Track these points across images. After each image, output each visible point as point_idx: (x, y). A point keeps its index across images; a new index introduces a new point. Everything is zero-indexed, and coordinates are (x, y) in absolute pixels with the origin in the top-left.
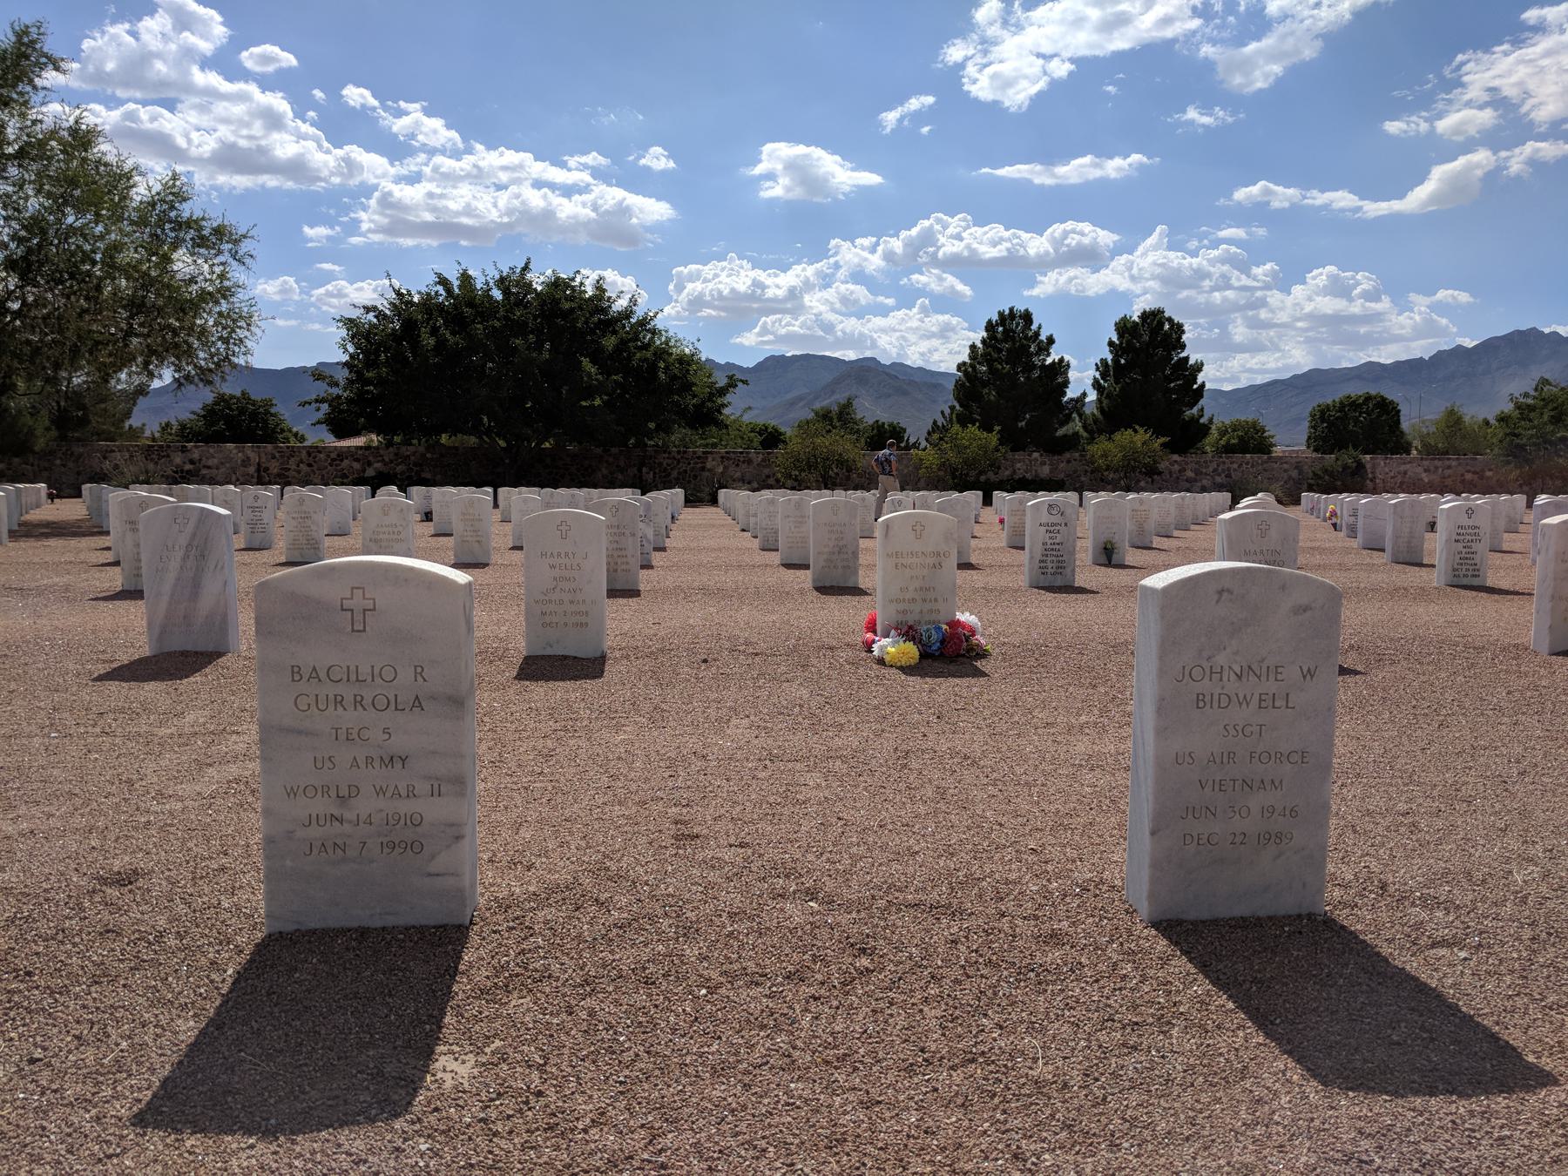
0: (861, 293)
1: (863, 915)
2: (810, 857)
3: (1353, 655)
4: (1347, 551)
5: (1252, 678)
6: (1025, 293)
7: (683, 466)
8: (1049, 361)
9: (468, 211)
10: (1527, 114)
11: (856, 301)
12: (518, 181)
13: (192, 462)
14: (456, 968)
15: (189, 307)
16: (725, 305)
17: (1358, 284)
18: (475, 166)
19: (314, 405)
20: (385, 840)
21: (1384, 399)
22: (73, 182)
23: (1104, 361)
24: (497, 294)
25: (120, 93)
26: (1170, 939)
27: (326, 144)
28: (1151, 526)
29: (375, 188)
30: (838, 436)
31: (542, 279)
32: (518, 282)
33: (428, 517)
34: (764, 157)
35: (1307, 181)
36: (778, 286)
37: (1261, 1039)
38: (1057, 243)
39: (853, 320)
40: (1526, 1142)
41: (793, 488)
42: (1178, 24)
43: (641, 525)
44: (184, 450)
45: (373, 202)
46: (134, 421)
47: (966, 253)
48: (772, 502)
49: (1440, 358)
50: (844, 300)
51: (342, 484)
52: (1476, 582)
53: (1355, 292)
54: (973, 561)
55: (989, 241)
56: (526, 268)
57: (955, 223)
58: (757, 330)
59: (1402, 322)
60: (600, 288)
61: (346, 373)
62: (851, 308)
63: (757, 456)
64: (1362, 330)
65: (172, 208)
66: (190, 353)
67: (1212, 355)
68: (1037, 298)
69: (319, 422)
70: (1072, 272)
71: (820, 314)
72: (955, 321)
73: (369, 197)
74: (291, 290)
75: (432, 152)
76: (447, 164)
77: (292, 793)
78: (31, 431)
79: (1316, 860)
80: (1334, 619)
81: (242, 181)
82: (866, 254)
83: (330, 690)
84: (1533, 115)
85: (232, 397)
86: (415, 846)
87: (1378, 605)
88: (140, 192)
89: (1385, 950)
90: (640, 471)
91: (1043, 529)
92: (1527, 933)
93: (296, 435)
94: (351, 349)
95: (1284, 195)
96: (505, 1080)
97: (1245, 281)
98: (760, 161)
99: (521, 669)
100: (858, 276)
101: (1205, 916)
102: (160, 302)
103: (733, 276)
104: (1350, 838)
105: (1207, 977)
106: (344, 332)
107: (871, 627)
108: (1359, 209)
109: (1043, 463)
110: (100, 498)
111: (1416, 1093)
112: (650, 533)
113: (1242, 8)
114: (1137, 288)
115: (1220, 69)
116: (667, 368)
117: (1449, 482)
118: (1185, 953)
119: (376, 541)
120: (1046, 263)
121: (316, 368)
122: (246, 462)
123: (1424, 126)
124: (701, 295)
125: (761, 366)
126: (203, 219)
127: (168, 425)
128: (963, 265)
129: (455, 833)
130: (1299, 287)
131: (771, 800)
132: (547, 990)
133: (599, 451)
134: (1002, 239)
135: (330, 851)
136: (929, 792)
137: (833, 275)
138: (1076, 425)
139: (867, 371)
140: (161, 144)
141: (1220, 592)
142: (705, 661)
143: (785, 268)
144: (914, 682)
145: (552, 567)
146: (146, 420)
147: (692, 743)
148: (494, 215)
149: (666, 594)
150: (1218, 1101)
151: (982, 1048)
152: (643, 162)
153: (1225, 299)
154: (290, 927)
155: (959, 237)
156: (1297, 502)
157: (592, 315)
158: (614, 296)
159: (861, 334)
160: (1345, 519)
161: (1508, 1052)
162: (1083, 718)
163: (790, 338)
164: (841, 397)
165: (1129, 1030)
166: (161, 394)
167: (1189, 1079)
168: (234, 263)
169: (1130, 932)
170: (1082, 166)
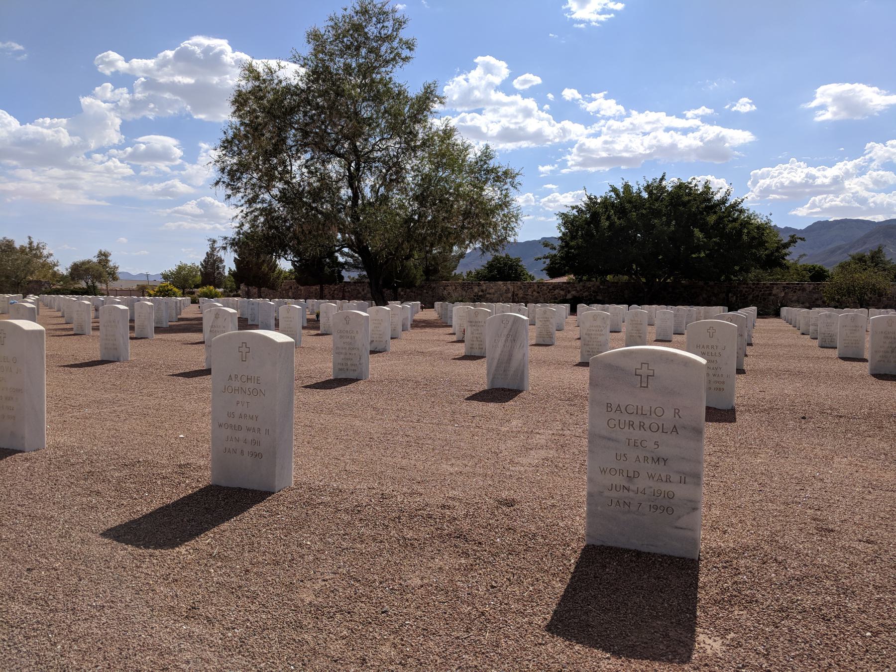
9: (626, 149)
11: (885, 182)
13: (482, 291)
18: (631, 124)
20: (652, 504)
22: (443, 156)
24: (645, 195)
25: (459, 110)
27: (553, 122)
29: (576, 142)
32: (657, 187)
34: (818, 95)
36: (825, 177)
39: (882, 195)
41: (836, 307)
44: (479, 285)
45: (574, 150)
46: (457, 271)
48: (854, 319)
50: (876, 182)
56: (662, 179)
58: (808, 205)
63: (809, 286)
65: (485, 163)
66: (489, 236)
71: (857, 192)
73: (572, 147)
74: (531, 200)
75: (608, 119)
76: (615, 124)
77: (603, 471)
78: (415, 277)
81: (510, 146)
83: (626, 418)
85: (501, 257)
86: (669, 510)
88: (471, 157)
90: (727, 295)
94: (563, 229)
98: (815, 98)
103: (795, 172)
106: (560, 221)
110: (447, 309)
116: (748, 233)
122: (507, 291)
124: (769, 186)
125: (810, 229)
127: (470, 272)
133: (701, 283)
135: (622, 505)
137: (868, 166)
140: (476, 132)
142: (804, 418)
143: (831, 165)
146: (461, 270)
148: (641, 150)
149: (763, 373)
152: (734, 109)
154: (598, 543)
163: (831, 210)
166: (471, 257)
168: (512, 188)
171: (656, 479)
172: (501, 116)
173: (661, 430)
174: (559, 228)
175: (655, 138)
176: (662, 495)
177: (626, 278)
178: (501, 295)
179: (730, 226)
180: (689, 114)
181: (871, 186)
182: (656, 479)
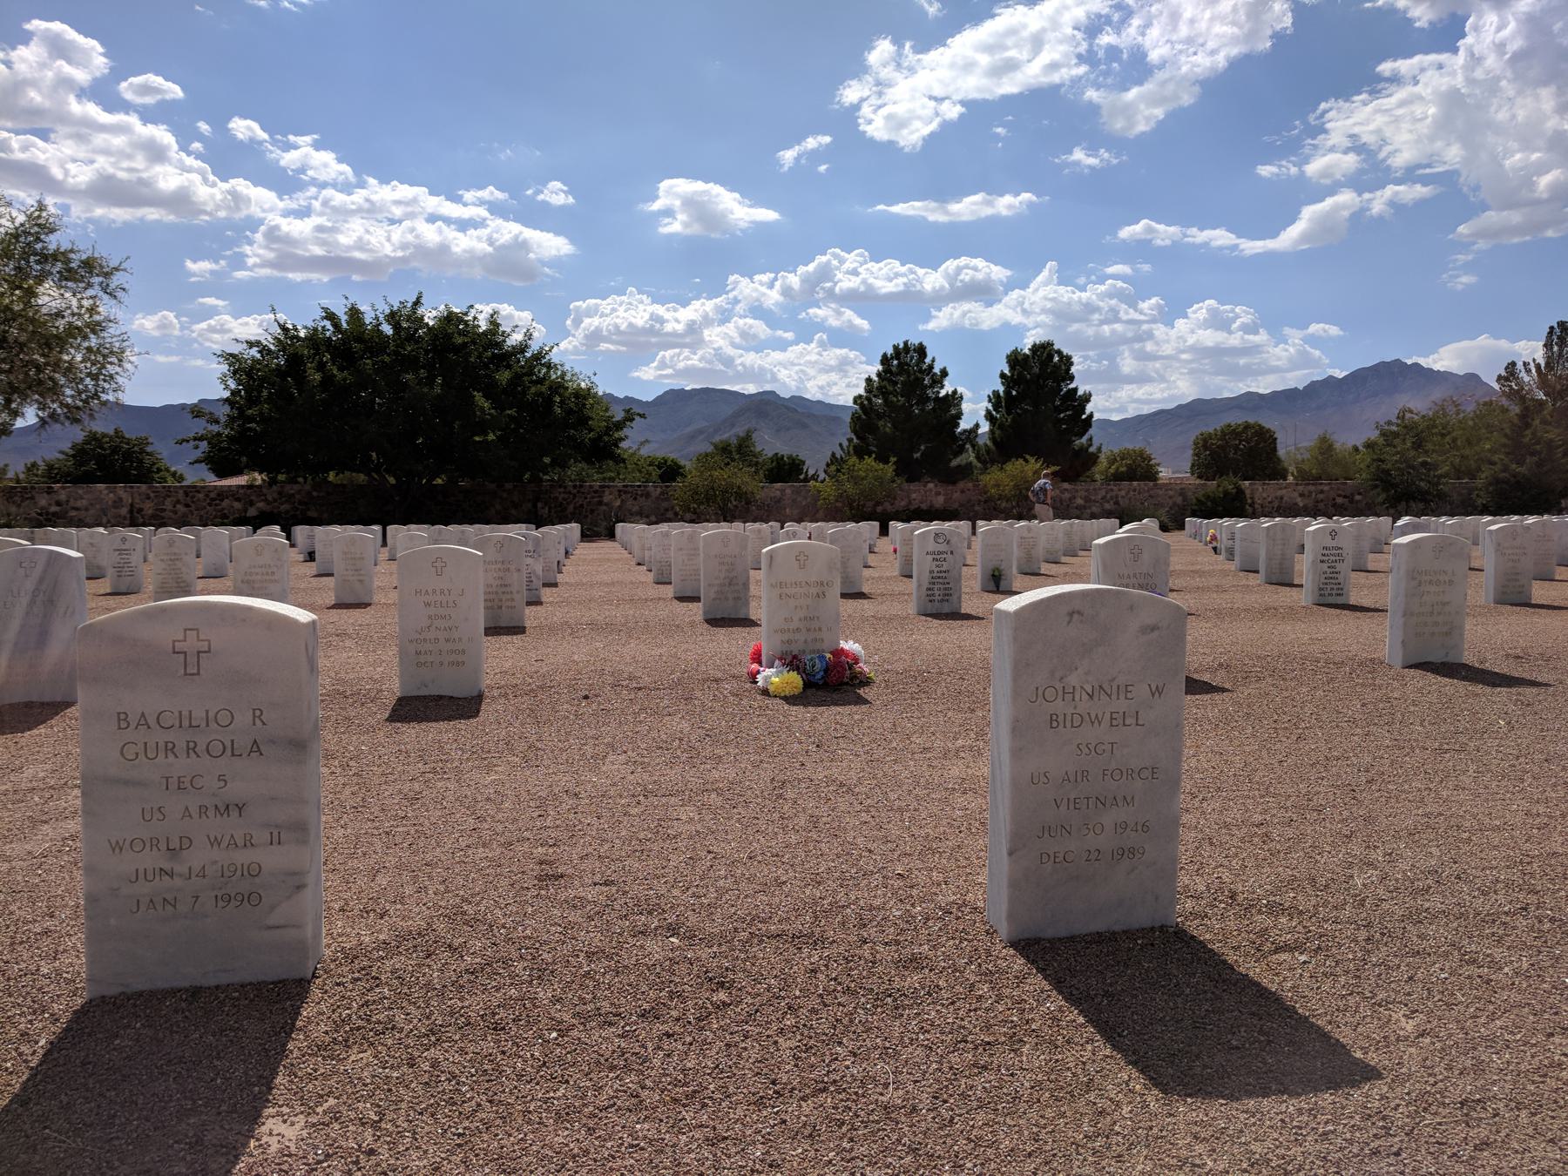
0: (760, 328)
1: (724, 948)
2: (676, 892)
3: (1222, 673)
4: (1225, 573)
5: (1104, 697)
6: (921, 327)
7: (579, 500)
8: (943, 393)
10: (1384, 160)
11: (755, 336)
12: (411, 216)
13: (58, 504)
14: (293, 1025)
15: (54, 342)
16: (625, 339)
17: (1238, 317)
18: (367, 200)
19: (192, 443)
23: (996, 393)
24: (387, 329)
26: (1027, 958)
27: (212, 178)
28: (1040, 552)
29: (261, 222)
30: (738, 466)
31: (434, 313)
33: (311, 557)
35: (1186, 223)
36: (677, 321)
37: (1108, 1052)
38: (952, 279)
40: (1348, 1136)
42: (1064, 70)
43: (529, 561)
44: (50, 491)
45: (259, 237)
47: (862, 289)
48: (667, 535)
49: (1313, 388)
50: (744, 334)
51: (222, 524)
52: (1340, 600)
53: (1234, 326)
54: (865, 590)
55: (886, 276)
56: (417, 303)
57: (852, 259)
59: (1280, 354)
60: (494, 323)
61: (227, 409)
62: (750, 342)
63: (655, 489)
64: (1242, 362)
65: (38, 240)
66: (55, 390)
67: (1101, 387)
68: (932, 332)
69: (197, 461)
70: (966, 306)
72: (852, 355)
73: (255, 231)
75: (323, 185)
76: (339, 198)
77: (117, 847)
79: (1168, 871)
80: (1180, 638)
81: (120, 214)
82: (763, 289)
84: (1389, 162)
85: (104, 435)
86: (251, 898)
89: (1231, 958)
90: (535, 506)
91: (930, 557)
92: (1363, 935)
93: (174, 474)
95: (1166, 232)
96: (335, 1141)
98: (656, 197)
99: (393, 710)
100: (757, 311)
101: (1063, 933)
102: (23, 338)
103: (633, 310)
104: (1207, 850)
105: (1060, 992)
106: (225, 368)
107: (757, 658)
108: (1236, 247)
109: (938, 494)
111: (1250, 1095)
112: (539, 568)
113: (1125, 56)
114: (1029, 322)
115: (1104, 112)
116: (562, 402)
117: (1321, 506)
118: (1041, 970)
119: (248, 582)
120: (941, 299)
121: (195, 405)
122: (118, 503)
123: (1294, 170)
124: (598, 330)
126: (72, 251)
127: (34, 465)
128: (861, 300)
129: (296, 882)
130: (1182, 321)
131: (641, 836)
132: (390, 1042)
133: (493, 486)
134: (897, 275)
135: (159, 908)
136: (802, 821)
138: (970, 456)
139: (767, 405)
141: (1071, 614)
142: (586, 697)
143: (685, 303)
144: (797, 711)
145: (428, 604)
147: (565, 781)
148: (388, 250)
149: (552, 630)
150: (1063, 1115)
151: (833, 1077)
152: (541, 197)
153: (1113, 332)
154: (113, 991)
155: (855, 273)
156: (1181, 527)
157: (485, 350)
158: (508, 330)
159: (761, 368)
160: (1223, 543)
161: (1339, 1049)
162: (960, 742)
163: (689, 372)
164: (740, 430)
165: (981, 1049)
167: (1036, 1095)
168: (106, 297)
169: (988, 953)
170: (974, 204)
171: (224, 845)
172: (95, 151)
173: (229, 752)
174: (224, 381)
175: (412, 230)
176: (239, 873)
177: (362, 478)
178: (104, 512)
179: (533, 390)
180: (469, 196)
181: (738, 340)
182: (224, 845)
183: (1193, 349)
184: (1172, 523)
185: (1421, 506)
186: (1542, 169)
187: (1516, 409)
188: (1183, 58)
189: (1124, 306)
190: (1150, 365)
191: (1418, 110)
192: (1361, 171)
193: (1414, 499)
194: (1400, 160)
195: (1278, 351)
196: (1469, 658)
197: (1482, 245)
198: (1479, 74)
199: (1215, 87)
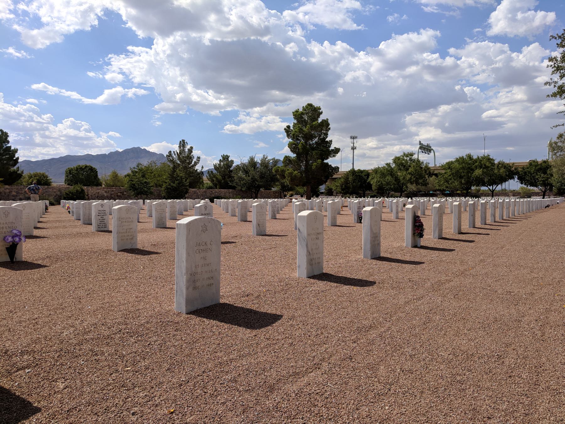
4: (70, 221)
10: (131, 79)
21: (92, 167)
35: (60, 85)
49: (111, 154)
52: (106, 229)
53: (82, 129)
59: (100, 141)
64: (85, 142)
84: (133, 80)
87: (68, 239)
95: (52, 90)
97: (39, 119)
108: (80, 100)
117: (113, 196)
123: (101, 76)
153: (31, 125)
156: (59, 204)
183: (65, 136)
184: (56, 202)
185: (145, 196)
186: (178, 92)
187: (172, 166)
188: (56, 24)
189: (35, 115)
190: (48, 140)
191: (141, 65)
192: (124, 81)
193: (144, 194)
194: (137, 80)
195: (98, 140)
196: (139, 246)
197: (162, 113)
198: (158, 58)
199: (70, 38)
